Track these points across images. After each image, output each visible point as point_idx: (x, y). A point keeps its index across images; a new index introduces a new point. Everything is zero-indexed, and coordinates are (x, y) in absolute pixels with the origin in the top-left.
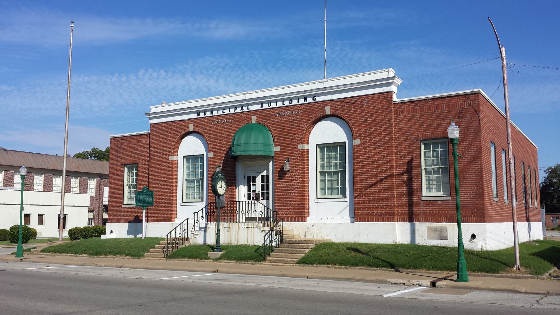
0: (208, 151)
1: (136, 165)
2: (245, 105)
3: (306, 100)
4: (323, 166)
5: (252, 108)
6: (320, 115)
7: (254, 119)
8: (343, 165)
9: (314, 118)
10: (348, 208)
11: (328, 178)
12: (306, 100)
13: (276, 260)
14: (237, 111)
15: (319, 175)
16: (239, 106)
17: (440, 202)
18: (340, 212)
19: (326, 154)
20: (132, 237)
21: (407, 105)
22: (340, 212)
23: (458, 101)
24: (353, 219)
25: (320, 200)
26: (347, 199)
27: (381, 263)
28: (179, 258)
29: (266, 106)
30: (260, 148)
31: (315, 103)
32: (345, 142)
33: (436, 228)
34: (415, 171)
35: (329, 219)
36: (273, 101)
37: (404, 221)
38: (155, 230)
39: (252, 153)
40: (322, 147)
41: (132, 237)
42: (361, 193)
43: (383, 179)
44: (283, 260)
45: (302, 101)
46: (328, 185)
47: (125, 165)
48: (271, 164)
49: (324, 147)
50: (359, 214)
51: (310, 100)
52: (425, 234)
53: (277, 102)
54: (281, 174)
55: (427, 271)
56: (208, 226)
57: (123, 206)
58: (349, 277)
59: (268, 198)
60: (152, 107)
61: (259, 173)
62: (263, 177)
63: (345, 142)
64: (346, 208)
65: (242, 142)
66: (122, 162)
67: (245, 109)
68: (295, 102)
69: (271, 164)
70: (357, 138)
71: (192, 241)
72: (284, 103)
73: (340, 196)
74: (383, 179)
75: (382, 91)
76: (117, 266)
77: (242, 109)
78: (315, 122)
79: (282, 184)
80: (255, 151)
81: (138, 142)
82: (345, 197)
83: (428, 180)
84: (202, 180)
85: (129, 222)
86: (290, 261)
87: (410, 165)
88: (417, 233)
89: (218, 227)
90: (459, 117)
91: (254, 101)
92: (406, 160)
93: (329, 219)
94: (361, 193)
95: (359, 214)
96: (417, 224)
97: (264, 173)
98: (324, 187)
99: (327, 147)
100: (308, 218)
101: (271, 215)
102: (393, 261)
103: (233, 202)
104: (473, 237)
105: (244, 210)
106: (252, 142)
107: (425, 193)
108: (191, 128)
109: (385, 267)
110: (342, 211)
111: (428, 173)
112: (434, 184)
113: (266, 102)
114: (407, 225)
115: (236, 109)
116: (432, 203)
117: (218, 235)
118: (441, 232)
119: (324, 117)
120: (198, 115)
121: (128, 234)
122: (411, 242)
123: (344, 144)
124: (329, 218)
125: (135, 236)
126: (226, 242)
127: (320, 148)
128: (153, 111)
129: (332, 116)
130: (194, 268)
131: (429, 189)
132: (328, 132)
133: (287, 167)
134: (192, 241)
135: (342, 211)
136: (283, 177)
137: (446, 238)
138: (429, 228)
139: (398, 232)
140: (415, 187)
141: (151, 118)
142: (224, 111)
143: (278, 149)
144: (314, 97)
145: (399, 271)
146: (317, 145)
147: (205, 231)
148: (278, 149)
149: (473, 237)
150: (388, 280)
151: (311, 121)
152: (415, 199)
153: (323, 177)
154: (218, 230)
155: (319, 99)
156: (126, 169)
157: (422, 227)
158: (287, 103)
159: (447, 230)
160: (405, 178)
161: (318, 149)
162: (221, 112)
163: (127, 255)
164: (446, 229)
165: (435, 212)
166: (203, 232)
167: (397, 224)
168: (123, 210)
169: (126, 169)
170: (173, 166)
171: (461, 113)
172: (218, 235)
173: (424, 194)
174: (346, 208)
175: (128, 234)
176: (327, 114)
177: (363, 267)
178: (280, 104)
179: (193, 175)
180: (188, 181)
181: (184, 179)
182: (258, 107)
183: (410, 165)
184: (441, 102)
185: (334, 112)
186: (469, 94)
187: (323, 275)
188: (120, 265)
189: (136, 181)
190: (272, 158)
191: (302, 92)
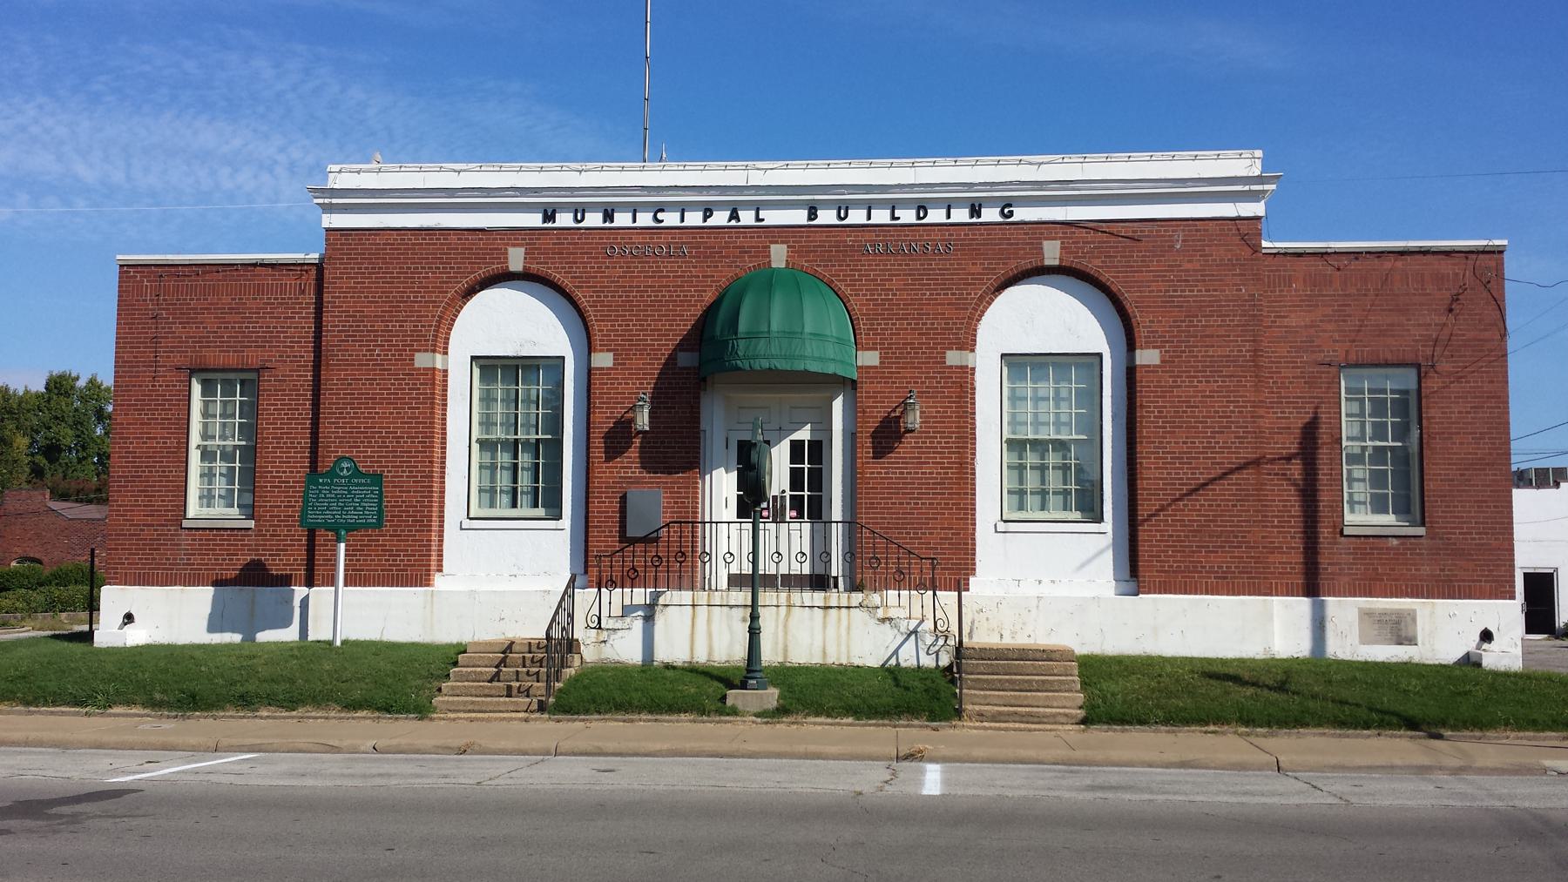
0: (587, 342)
1: (253, 376)
2: (747, 205)
3: (975, 211)
4: (487, 423)
5: (772, 217)
6: (1026, 264)
7: (779, 255)
8: (555, 423)
9: (1002, 272)
10: (1109, 555)
11: (1031, 458)
12: (975, 211)
13: (1000, 713)
14: (711, 222)
15: (476, 447)
16: (721, 205)
17: (1395, 542)
18: (1083, 566)
19: (499, 389)
20: (237, 638)
21: (1303, 262)
22: (1083, 566)
23: (1446, 267)
24: (1132, 585)
25: (1012, 527)
26: (1107, 526)
27: (1395, 720)
28: (1319, 725)
29: (827, 217)
30: (830, 352)
31: (1007, 225)
32: (1100, 355)
33: (1384, 613)
34: (1323, 454)
35: (1045, 583)
36: (858, 204)
37: (1289, 592)
38: (351, 613)
39: (814, 367)
40: (488, 366)
41: (237, 638)
42: (1163, 509)
43: (1232, 471)
44: (1030, 715)
45: (961, 215)
46: (1032, 479)
47: (193, 372)
48: (838, 405)
49: (496, 367)
50: (1137, 571)
51: (990, 215)
52: (1351, 630)
53: (635, 210)
54: (886, 436)
55: (1521, 734)
56: (661, 601)
57: (185, 524)
58: (1190, 757)
59: (816, 511)
60: (335, 168)
61: (782, 432)
62: (796, 447)
63: (1100, 355)
64: (1101, 552)
65: (775, 327)
66: (178, 359)
67: (747, 217)
68: (936, 216)
69: (838, 405)
70: (1150, 345)
71: (589, 654)
72: (762, 214)
73: (1077, 515)
74: (1232, 471)
75: (1234, 214)
76: (447, 749)
77: (734, 216)
78: (470, 293)
79: (875, 470)
80: (820, 359)
81: (260, 289)
82: (1100, 519)
83: (208, 475)
84: (558, 444)
85: (216, 583)
86: (1054, 715)
87: (1310, 433)
88: (1329, 627)
89: (754, 605)
90: (1451, 310)
91: (786, 196)
92: (1298, 421)
93: (1045, 583)
94: (1163, 509)
95: (1137, 571)
96: (1331, 601)
97: (804, 434)
98: (1016, 486)
99: (504, 367)
100: (972, 579)
101: (836, 568)
102: (1413, 710)
103: (689, 522)
104: (129, 618)
105: (783, 550)
106: (808, 329)
107: (194, 508)
108: (516, 259)
109: (1390, 726)
110: (1089, 561)
111: (207, 455)
112: (220, 485)
113: (827, 205)
114: (1303, 604)
115: (708, 213)
116: (1371, 542)
117: (754, 632)
118: (1398, 623)
119: (1037, 272)
120: (813, 214)
121: (212, 628)
122: (1313, 651)
123: (557, 366)
124: (1046, 580)
125: (249, 638)
126: (724, 659)
127: (482, 368)
128: (343, 178)
129: (527, 278)
130: (812, 748)
131: (207, 498)
132: (1041, 318)
133: (914, 419)
134: (589, 654)
135: (1089, 561)
136: (891, 449)
137: (1411, 641)
138: (1366, 615)
139: (1277, 625)
140: (1324, 498)
141: (330, 209)
142: (660, 216)
143: (870, 358)
144: (1006, 206)
145: (1439, 737)
146: (473, 358)
147: (649, 619)
148: (870, 358)
149: (129, 618)
150: (1548, 763)
151: (992, 281)
152: (1325, 532)
153: (1015, 454)
154: (754, 617)
155: (1021, 214)
156: (197, 388)
157: (1344, 611)
158: (907, 216)
159: (1414, 620)
160: (1296, 469)
161: (477, 372)
162: (645, 219)
163: (352, 706)
164: (1412, 615)
165: (1381, 569)
166: (638, 625)
167: (1277, 602)
168: (185, 540)
169: (197, 388)
170: (433, 386)
171: (1455, 299)
172: (754, 632)
173: (191, 513)
174: (1101, 552)
175: (212, 628)
176: (1047, 262)
177: (1321, 730)
178: (881, 216)
179: (526, 425)
180: (485, 445)
181: (474, 439)
182: (799, 217)
183: (1310, 433)
184: (1399, 264)
185: (1075, 263)
186: (1478, 252)
187: (1333, 761)
188: (461, 742)
189: (249, 431)
190: (848, 385)
191: (571, 190)
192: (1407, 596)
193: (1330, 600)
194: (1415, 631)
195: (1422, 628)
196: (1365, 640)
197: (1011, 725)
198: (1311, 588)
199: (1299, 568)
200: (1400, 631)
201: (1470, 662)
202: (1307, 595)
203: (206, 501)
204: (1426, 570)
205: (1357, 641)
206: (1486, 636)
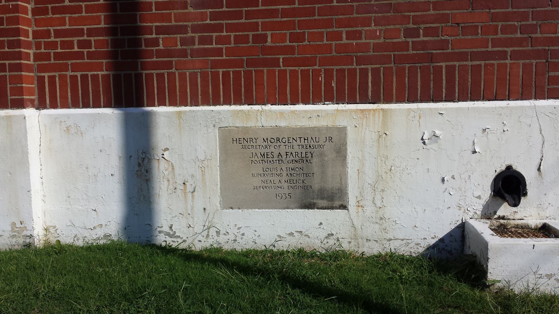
33: (276, 138)
88: (161, 171)
114: (103, 124)
118: (305, 159)
137: (334, 199)
138: (236, 142)
157: (191, 135)
159: (341, 152)
192: (329, 98)
193: (162, 112)
194: (343, 176)
195: (358, 171)
196: (233, 200)
197: (471, 24)
198: (128, 86)
199: (99, 43)
200: (311, 178)
201: (457, 258)
202: (116, 101)
203: (421, 31)
204: (374, 34)
205: (217, 200)
206: (509, 186)
